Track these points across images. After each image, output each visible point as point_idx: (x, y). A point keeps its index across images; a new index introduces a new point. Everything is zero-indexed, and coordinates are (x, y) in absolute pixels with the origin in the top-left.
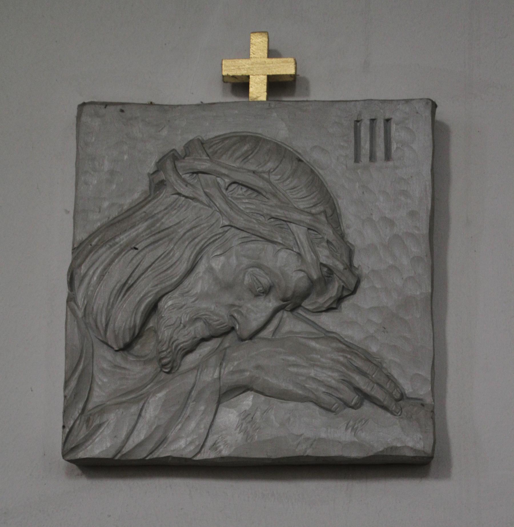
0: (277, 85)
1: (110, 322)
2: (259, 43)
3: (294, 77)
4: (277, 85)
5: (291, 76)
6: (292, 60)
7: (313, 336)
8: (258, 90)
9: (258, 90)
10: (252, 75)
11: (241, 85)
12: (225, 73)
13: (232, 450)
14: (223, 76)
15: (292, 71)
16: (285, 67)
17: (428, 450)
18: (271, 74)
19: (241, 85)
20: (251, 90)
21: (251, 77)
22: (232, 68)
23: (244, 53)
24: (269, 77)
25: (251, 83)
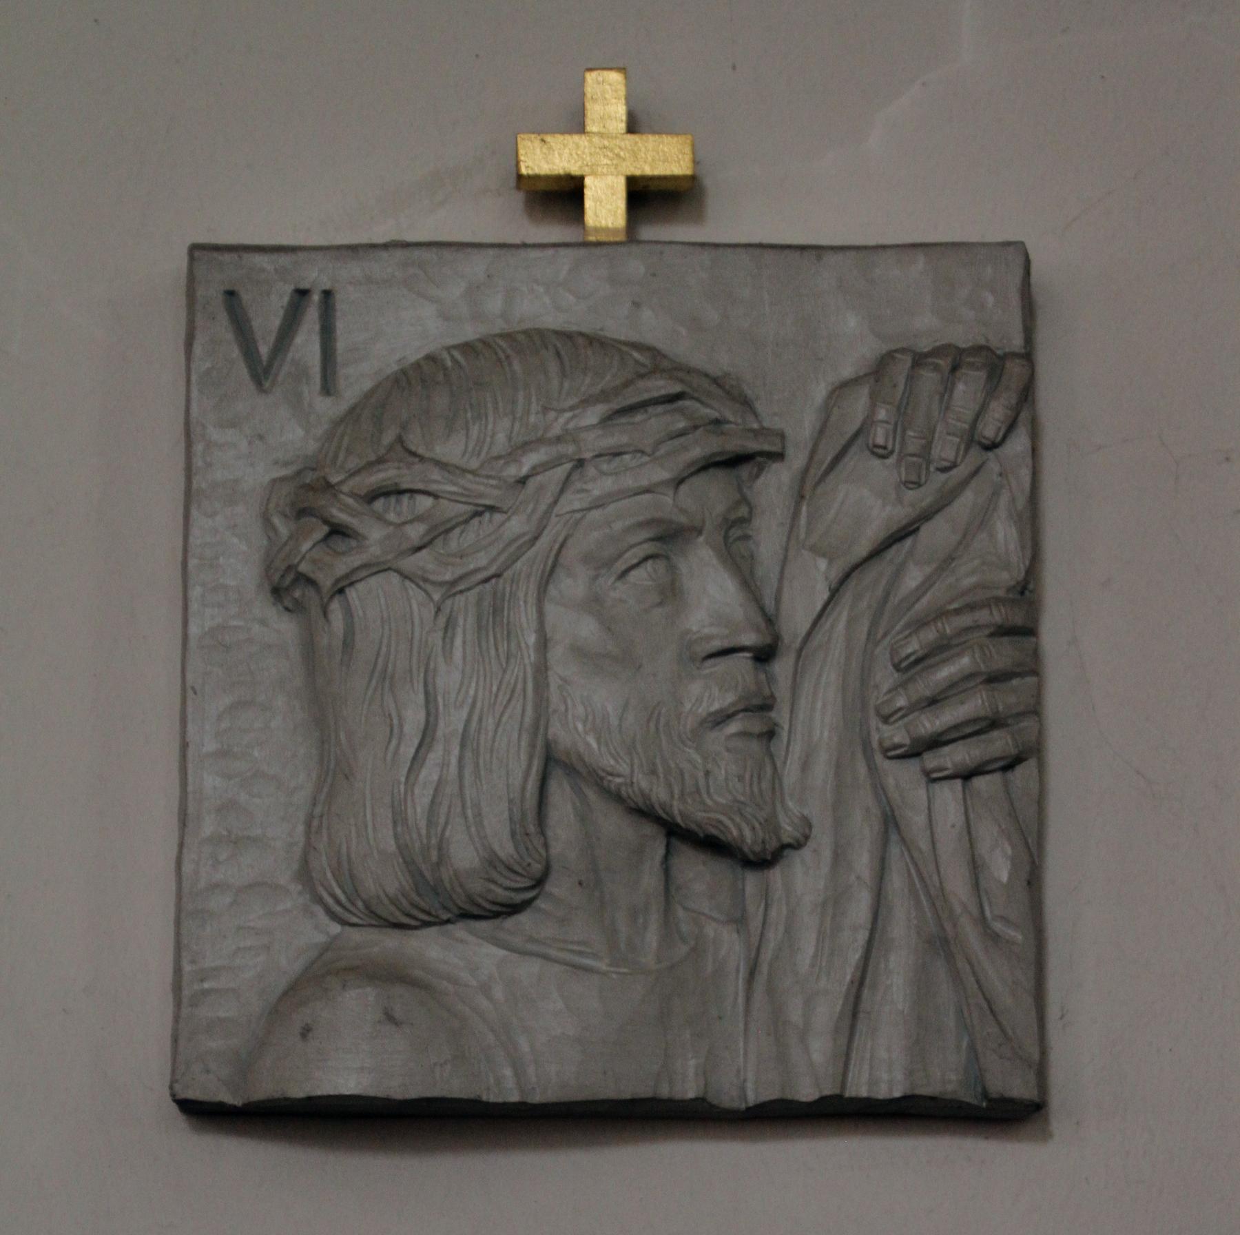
0: (645, 196)
1: (546, 532)
2: (607, 97)
3: (693, 178)
4: (645, 196)
5: (684, 178)
6: (591, 77)
7: (977, 727)
8: (605, 207)
9: (605, 207)
10: (594, 173)
11: (565, 195)
12: (524, 171)
13: (740, 688)
14: (520, 177)
15: (689, 172)
16: (665, 157)
17: (768, 640)
18: (638, 173)
19: (565, 195)
20: (588, 204)
21: (588, 181)
22: (545, 157)
23: (575, 122)
24: (632, 181)
25: (588, 193)
